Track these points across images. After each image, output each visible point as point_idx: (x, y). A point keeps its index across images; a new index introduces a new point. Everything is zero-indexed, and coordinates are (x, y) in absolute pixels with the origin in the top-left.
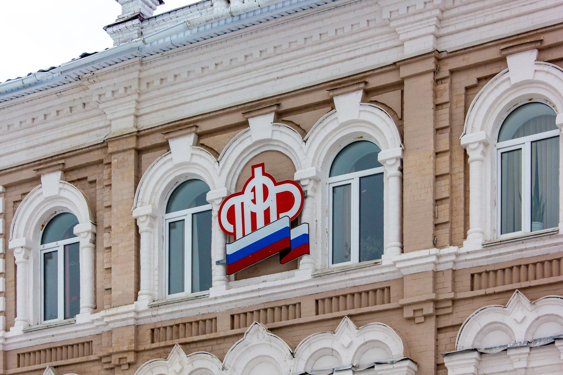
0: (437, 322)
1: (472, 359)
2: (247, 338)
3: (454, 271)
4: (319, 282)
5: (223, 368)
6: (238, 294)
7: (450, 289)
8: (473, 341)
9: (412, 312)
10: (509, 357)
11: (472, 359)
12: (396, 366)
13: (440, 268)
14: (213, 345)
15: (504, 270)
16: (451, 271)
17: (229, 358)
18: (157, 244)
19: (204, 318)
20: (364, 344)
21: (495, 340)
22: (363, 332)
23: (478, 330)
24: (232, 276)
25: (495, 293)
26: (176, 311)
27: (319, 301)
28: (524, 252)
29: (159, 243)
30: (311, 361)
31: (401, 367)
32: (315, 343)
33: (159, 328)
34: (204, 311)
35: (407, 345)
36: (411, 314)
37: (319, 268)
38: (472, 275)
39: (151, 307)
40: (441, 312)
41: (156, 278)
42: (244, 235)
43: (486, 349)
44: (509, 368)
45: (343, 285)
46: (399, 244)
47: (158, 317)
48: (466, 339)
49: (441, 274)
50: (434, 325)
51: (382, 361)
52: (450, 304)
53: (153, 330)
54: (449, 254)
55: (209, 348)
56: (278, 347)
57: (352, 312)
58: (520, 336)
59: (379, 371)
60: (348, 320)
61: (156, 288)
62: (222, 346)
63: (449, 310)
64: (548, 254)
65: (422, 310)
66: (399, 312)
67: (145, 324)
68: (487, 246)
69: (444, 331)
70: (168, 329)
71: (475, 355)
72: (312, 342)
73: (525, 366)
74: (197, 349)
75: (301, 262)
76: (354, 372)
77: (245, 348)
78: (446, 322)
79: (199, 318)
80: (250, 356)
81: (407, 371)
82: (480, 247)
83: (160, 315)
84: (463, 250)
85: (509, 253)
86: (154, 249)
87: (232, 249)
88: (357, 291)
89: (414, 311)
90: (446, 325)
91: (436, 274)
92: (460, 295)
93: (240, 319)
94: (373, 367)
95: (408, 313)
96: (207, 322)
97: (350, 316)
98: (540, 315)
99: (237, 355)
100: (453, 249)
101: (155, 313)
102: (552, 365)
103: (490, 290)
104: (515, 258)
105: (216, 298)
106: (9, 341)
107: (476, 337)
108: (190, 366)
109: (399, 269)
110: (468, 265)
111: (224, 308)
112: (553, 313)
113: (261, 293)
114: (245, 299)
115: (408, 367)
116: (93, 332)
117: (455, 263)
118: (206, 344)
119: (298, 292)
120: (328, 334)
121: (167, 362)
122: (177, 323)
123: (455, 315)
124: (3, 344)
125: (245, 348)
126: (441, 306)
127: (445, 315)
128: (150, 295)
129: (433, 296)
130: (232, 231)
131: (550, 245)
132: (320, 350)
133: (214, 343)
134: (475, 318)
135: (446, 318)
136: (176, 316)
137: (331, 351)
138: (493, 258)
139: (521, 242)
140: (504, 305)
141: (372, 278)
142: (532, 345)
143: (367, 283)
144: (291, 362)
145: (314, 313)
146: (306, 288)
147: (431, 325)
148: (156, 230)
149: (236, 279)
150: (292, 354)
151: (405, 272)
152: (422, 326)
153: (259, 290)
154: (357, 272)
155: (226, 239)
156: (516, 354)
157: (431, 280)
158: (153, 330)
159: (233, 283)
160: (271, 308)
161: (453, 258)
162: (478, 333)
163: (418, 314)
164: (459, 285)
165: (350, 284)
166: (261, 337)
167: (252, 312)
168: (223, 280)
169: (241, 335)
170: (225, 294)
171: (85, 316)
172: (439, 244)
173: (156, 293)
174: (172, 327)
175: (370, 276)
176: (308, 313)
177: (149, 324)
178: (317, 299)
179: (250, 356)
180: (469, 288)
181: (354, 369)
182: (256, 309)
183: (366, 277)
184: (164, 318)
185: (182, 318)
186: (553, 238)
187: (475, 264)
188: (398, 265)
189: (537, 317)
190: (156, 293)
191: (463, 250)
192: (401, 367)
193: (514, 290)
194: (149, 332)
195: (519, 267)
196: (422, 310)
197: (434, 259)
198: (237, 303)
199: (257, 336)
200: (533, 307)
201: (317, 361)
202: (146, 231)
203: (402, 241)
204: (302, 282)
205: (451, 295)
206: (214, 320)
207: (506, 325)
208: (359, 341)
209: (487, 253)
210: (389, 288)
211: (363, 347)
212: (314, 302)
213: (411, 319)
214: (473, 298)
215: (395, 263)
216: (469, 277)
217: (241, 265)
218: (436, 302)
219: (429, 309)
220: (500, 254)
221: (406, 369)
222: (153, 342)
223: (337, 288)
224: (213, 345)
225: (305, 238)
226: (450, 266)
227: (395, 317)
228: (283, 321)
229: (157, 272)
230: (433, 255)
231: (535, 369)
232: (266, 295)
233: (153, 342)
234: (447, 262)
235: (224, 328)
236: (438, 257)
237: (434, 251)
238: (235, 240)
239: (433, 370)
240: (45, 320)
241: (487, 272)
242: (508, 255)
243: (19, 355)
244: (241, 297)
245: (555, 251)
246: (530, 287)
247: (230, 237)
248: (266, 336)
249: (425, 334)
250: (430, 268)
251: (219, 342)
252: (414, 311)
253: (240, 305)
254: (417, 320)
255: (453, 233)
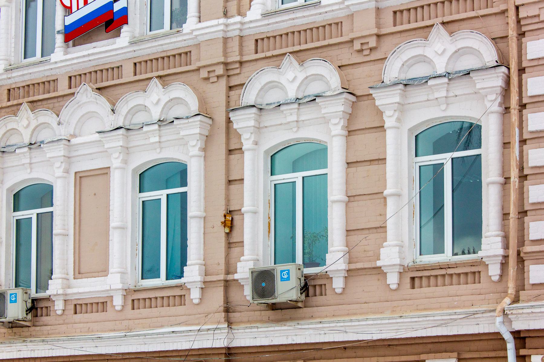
0: (228, 81)
1: (251, 114)
2: (78, 97)
3: (241, 37)
4: (135, 48)
5: (59, 123)
6: (73, 59)
7: (237, 53)
8: (256, 98)
9: (360, 45)
10: (282, 111)
11: (251, 114)
12: (191, 120)
13: (229, 35)
14: (54, 103)
15: (281, 35)
16: (238, 37)
17: (64, 113)
18: (14, 17)
19: (48, 79)
20: (169, 101)
21: (274, 97)
22: (168, 91)
23: (259, 89)
24: (71, 43)
25: (273, 56)
26: (26, 74)
27: (259, 40)
28: (295, 21)
29: (16, 14)
30: (129, 116)
31: (194, 122)
32: (131, 100)
33: (14, 89)
34: (47, 73)
35: (203, 101)
36: (206, 75)
37: (137, 35)
38: (257, 41)
39: (6, 70)
40: (231, 73)
41: (13, 45)
42: (78, 9)
43: (267, 104)
44: (284, 121)
45: (154, 50)
46: (197, 14)
47: (13, 79)
48: (250, 96)
49: (230, 40)
50: (225, 84)
51: (180, 117)
52: (237, 65)
53: (9, 90)
54: (235, 23)
55: (51, 106)
56: (101, 105)
57: (161, 73)
58: (292, 94)
59: (178, 124)
60: (156, 80)
61: (13, 54)
62: (61, 103)
63: (238, 71)
64: (314, 22)
65: (214, 71)
66: (197, 73)
67: (3, 85)
68: (266, 15)
69: (235, 89)
70: (21, 89)
71: (254, 110)
72: (129, 99)
73: (296, 119)
74: (42, 106)
75: (122, 30)
76: (160, 126)
77: (77, 105)
78: (235, 81)
79: (44, 80)
80: (80, 113)
81: (200, 124)
82: (259, 17)
83: (14, 77)
84: (246, 19)
85: (283, 21)
86: (11, 20)
87: (70, 20)
88: (166, 55)
89: (208, 72)
90: (236, 84)
91: (226, 40)
92: (245, 58)
93: (73, 80)
94: (173, 122)
95: (204, 73)
96: (49, 84)
97: (160, 77)
98: (308, 75)
99: (72, 112)
100: (238, 19)
101: (9, 76)
102: (317, 118)
103: (269, 54)
104: (290, 25)
105: (56, 63)
106: (247, 26)
107: (258, 94)
108: (35, 121)
109: (197, 36)
110: (251, 32)
111: (64, 71)
112: (318, 73)
113: (91, 58)
114: (79, 63)
115: (201, 121)
116: (191, 43)
117: (241, 30)
118: (44, 103)
119: (119, 56)
120: (141, 93)
121: (17, 118)
122: (28, 84)
123: (242, 75)
124: (223, 31)
125: (77, 105)
126: (230, 68)
127: (234, 75)
128: (7, 60)
129: (222, 59)
130: (69, 5)
131: (316, 14)
132: (135, 106)
133: (55, 100)
134: (256, 78)
135: (235, 78)
136: (26, 78)
137: (144, 107)
138: (271, 26)
139: (292, 12)
140: (278, 67)
141: (176, 44)
142: (301, 101)
143: (173, 48)
144: (112, 117)
145: (133, 74)
146: (125, 53)
147: (223, 83)
148: (14, 5)
149: (74, 45)
150: (113, 110)
151: (201, 39)
152: (215, 85)
153: (89, 55)
154: (164, 39)
155: (66, 12)
156: (287, 110)
157: (221, 45)
158: (9, 90)
159: (72, 49)
160: (100, 70)
161: (238, 26)
162: (260, 91)
163: (212, 75)
164: (245, 49)
165: (160, 49)
166: (89, 96)
167: (85, 74)
168: (62, 47)
169: (73, 94)
170: (65, 58)
171: (191, 24)
172: (229, 14)
173: (13, 59)
174: (24, 87)
175: (175, 42)
176: (128, 75)
177: (6, 85)
178: (135, 62)
179: (80, 113)
180: (254, 51)
181: (160, 123)
182: (88, 71)
183: (171, 43)
184: (17, 80)
185: (31, 80)
186: (318, 8)
187: (258, 30)
188: (195, 33)
189: (305, 76)
190: (13, 59)
191: (246, 19)
192: (194, 122)
193: (285, 54)
194: (6, 92)
195: (293, 33)
196: (214, 71)
197: (222, 27)
198: (73, 66)
199: (86, 95)
200: (302, 68)
201: (135, 116)
202: (4, 6)
203: (200, 12)
204: (122, 48)
205: (238, 58)
206: (188, 53)
207: (281, 84)
208: (165, 99)
209: (266, 22)
210: (190, 52)
211: (170, 103)
212: (132, 65)
213: (207, 79)
214: (256, 60)
215: (193, 31)
216: (253, 42)
217: (76, 34)
218: (226, 64)
219: (220, 70)
220: (277, 23)
221: (199, 123)
222: (9, 100)
223: (150, 53)
224: (54, 103)
225: (125, 10)
226: (237, 33)
227: (194, 77)
228: (107, 82)
229: (13, 40)
230: (221, 24)
231: (305, 122)
232: (94, 60)
233: (9, 100)
234: (234, 30)
235: (63, 88)
236: (227, 25)
237: (222, 20)
238: (72, 13)
239: (224, 123)
240: (25, 58)
241: (268, 38)
242: (283, 23)
243: (395, 12)
244: (75, 61)
245: (320, 19)
246: (300, 51)
247: (68, 10)
248: (93, 95)
249: (217, 92)
250: (221, 35)
251: (59, 99)
252: (362, 44)
253: (76, 67)
254: (212, 80)
255: (241, 4)
